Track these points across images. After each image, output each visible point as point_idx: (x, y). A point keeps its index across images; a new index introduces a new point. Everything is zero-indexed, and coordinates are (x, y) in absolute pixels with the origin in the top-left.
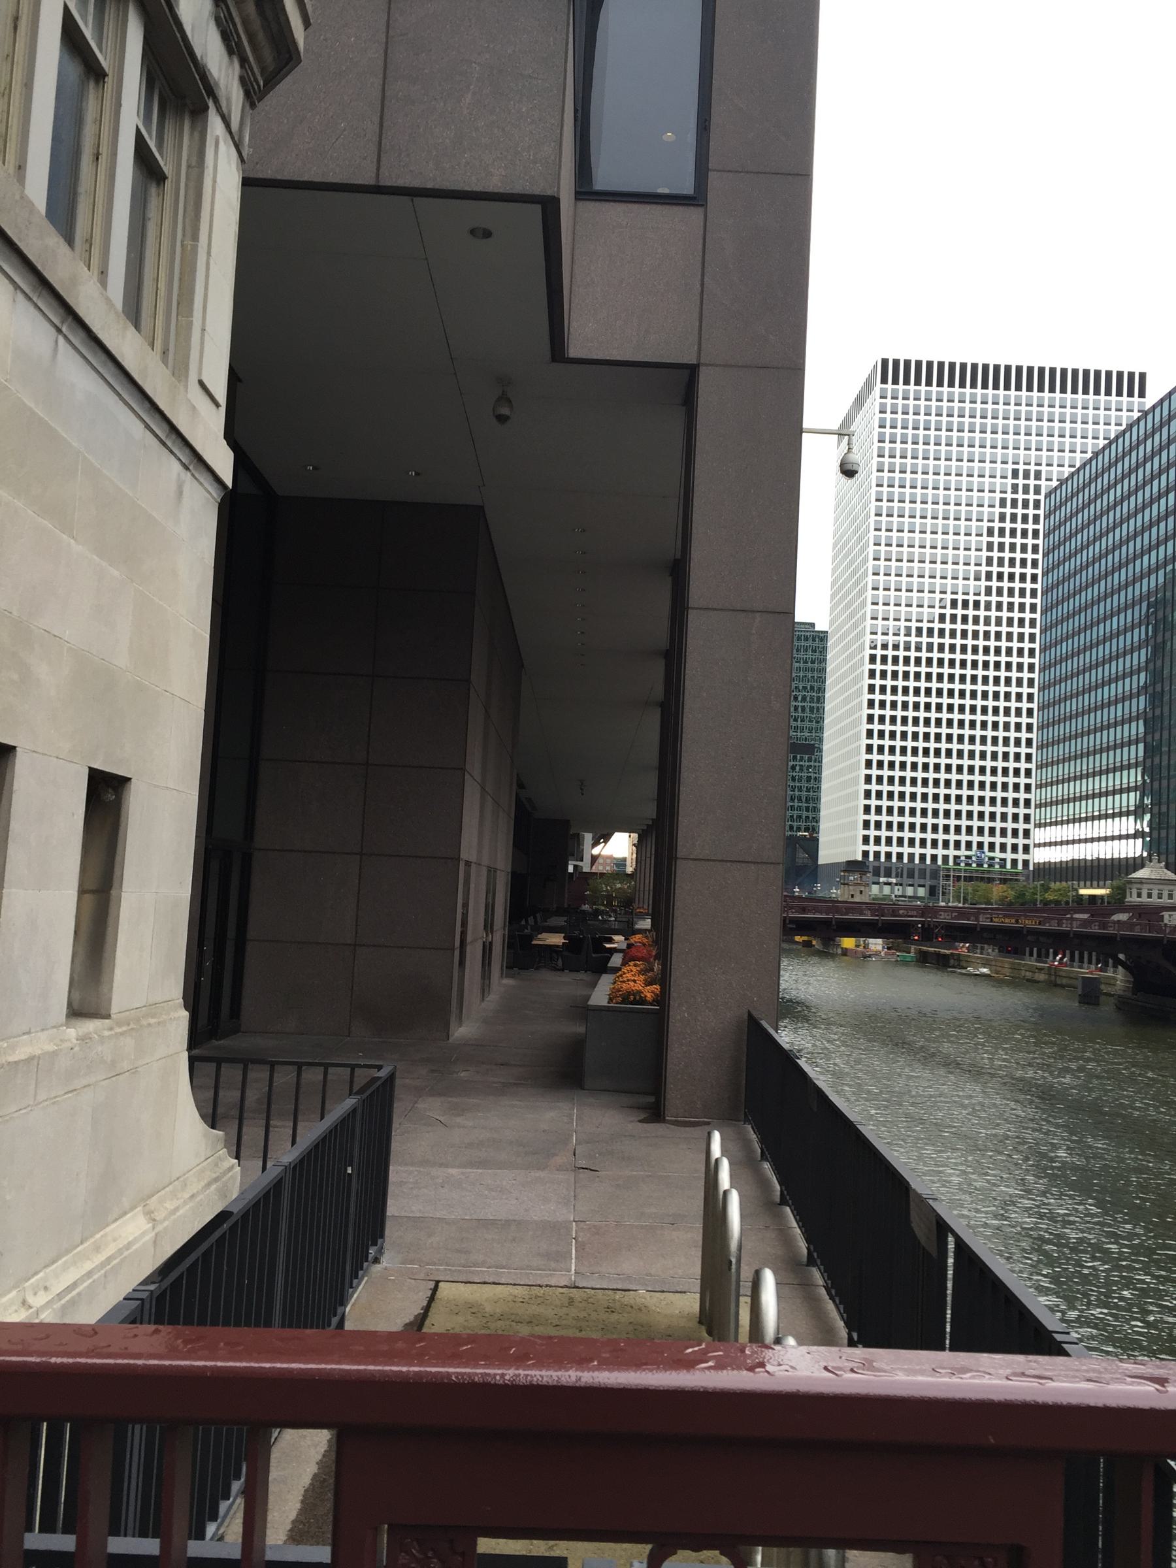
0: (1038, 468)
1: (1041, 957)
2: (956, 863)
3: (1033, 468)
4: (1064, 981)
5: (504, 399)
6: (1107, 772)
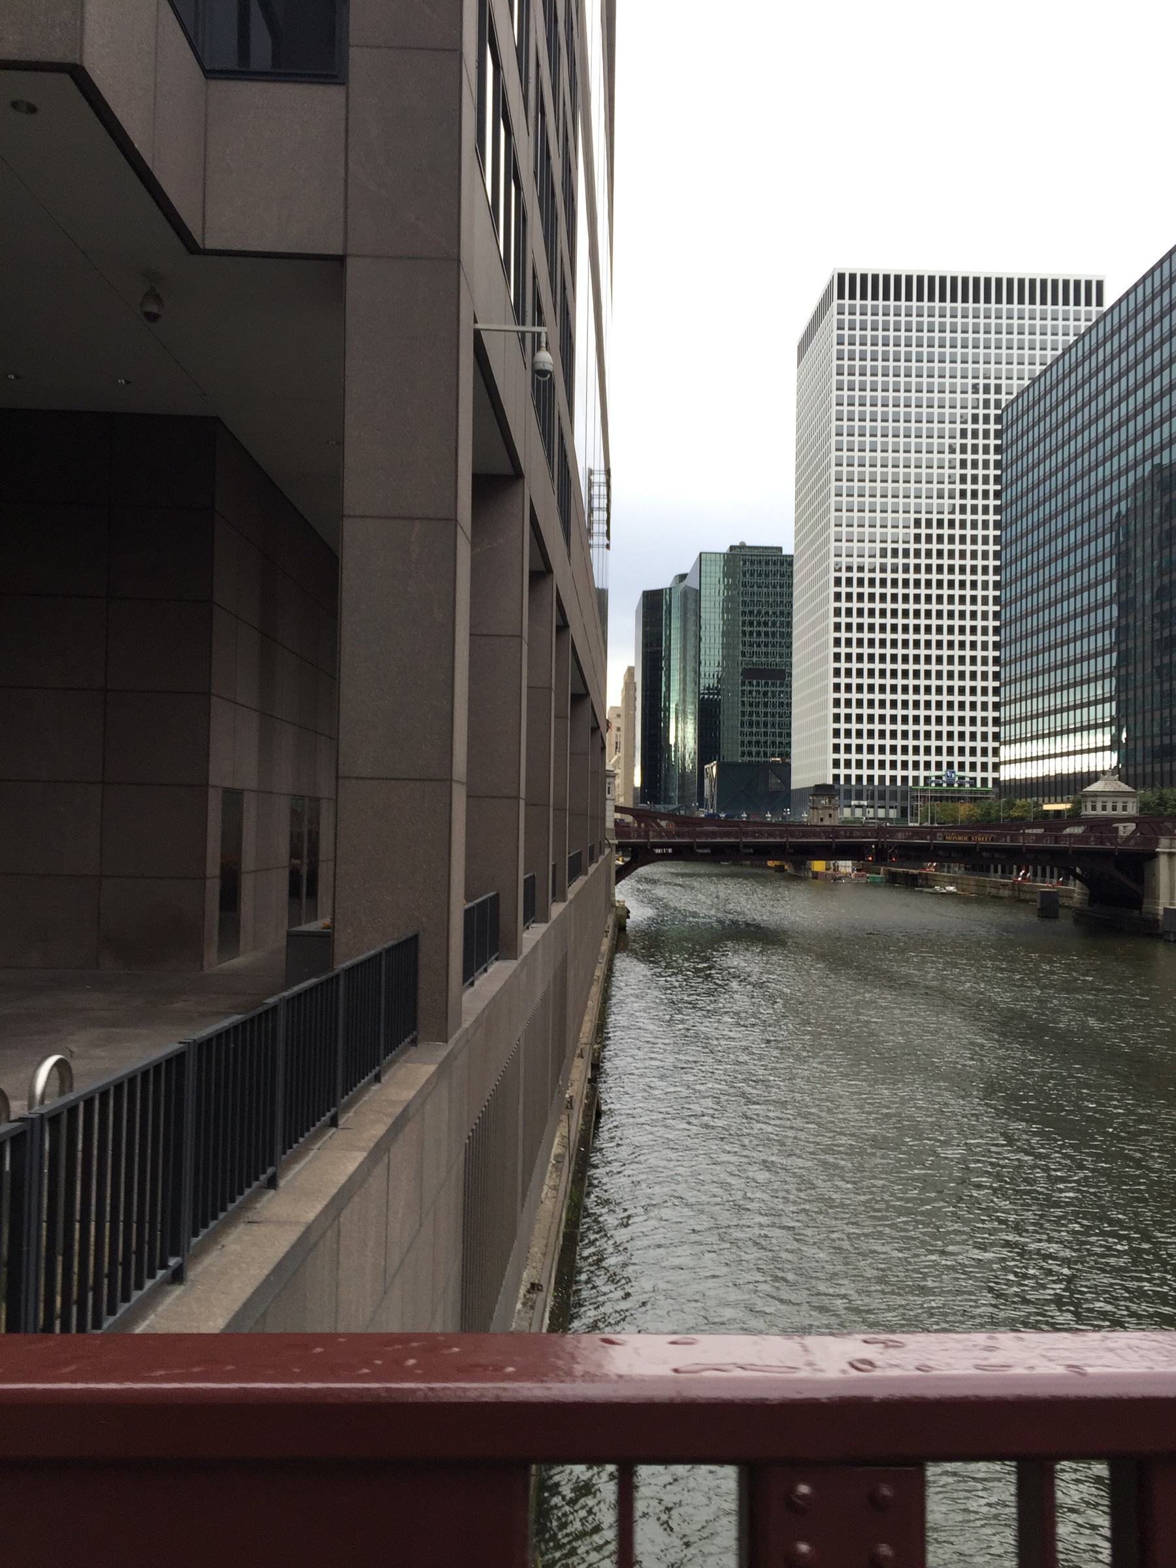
2: (926, 784)
3: (993, 382)
4: (1028, 896)
6: (1068, 687)
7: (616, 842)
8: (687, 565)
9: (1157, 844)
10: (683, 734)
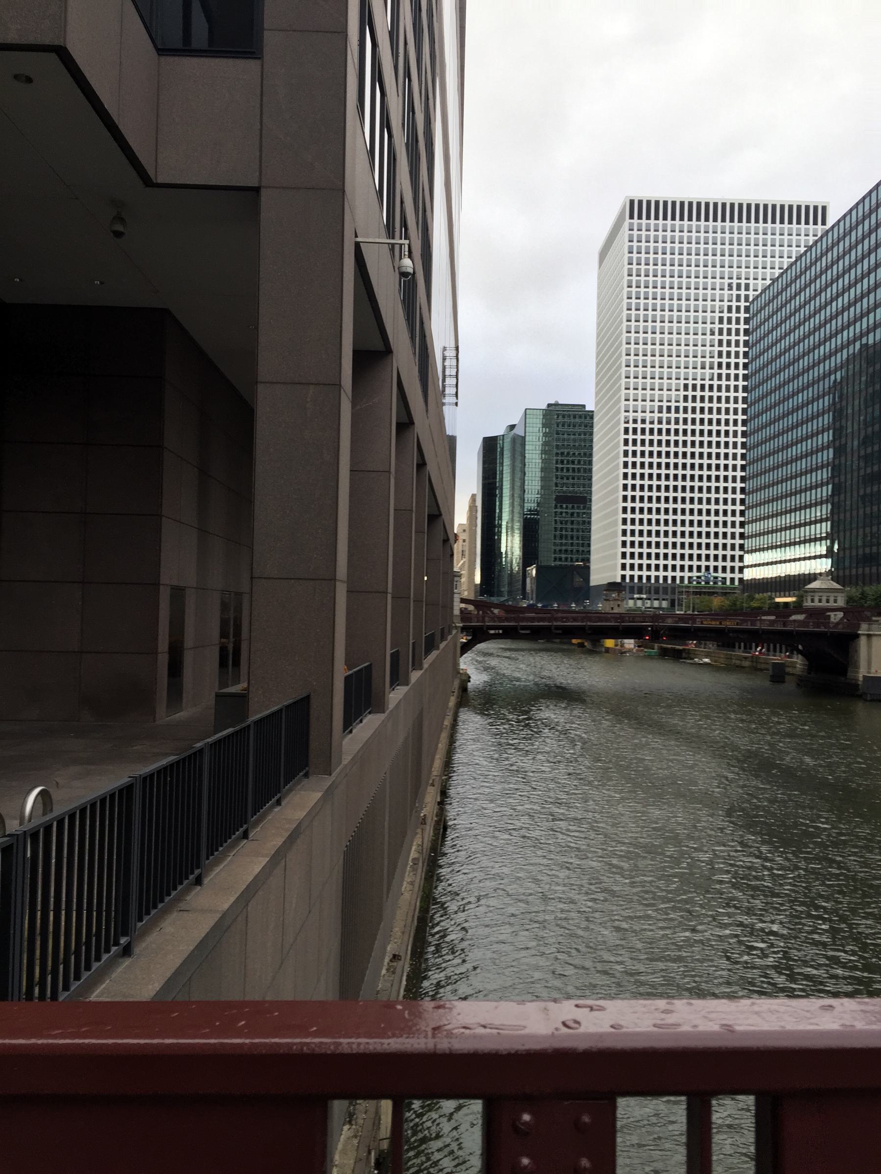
0: (747, 281)
1: (748, 648)
2: (690, 582)
3: (743, 282)
5: (120, 219)
7: (461, 625)
8: (516, 419)
9: (858, 628)
10: (511, 545)
